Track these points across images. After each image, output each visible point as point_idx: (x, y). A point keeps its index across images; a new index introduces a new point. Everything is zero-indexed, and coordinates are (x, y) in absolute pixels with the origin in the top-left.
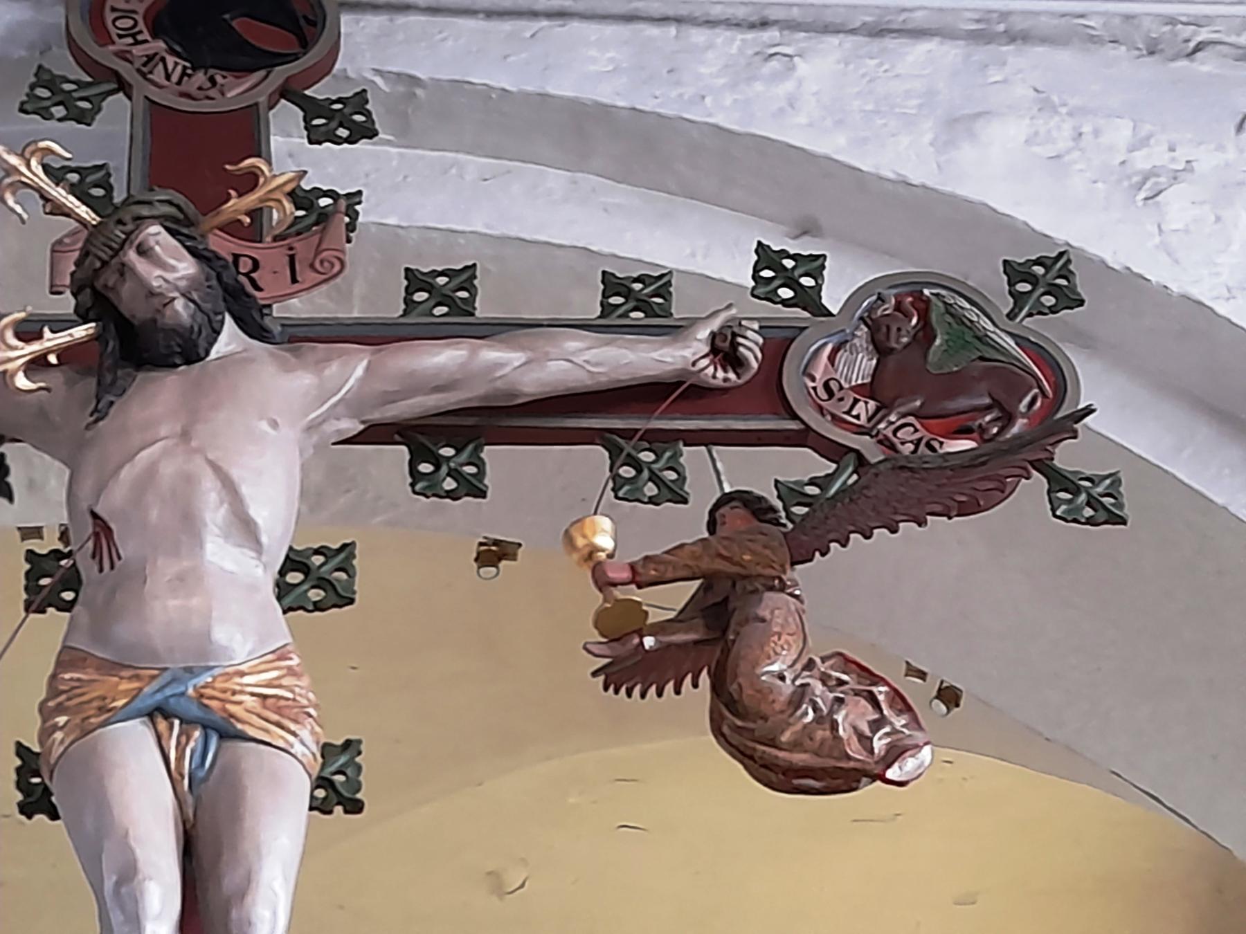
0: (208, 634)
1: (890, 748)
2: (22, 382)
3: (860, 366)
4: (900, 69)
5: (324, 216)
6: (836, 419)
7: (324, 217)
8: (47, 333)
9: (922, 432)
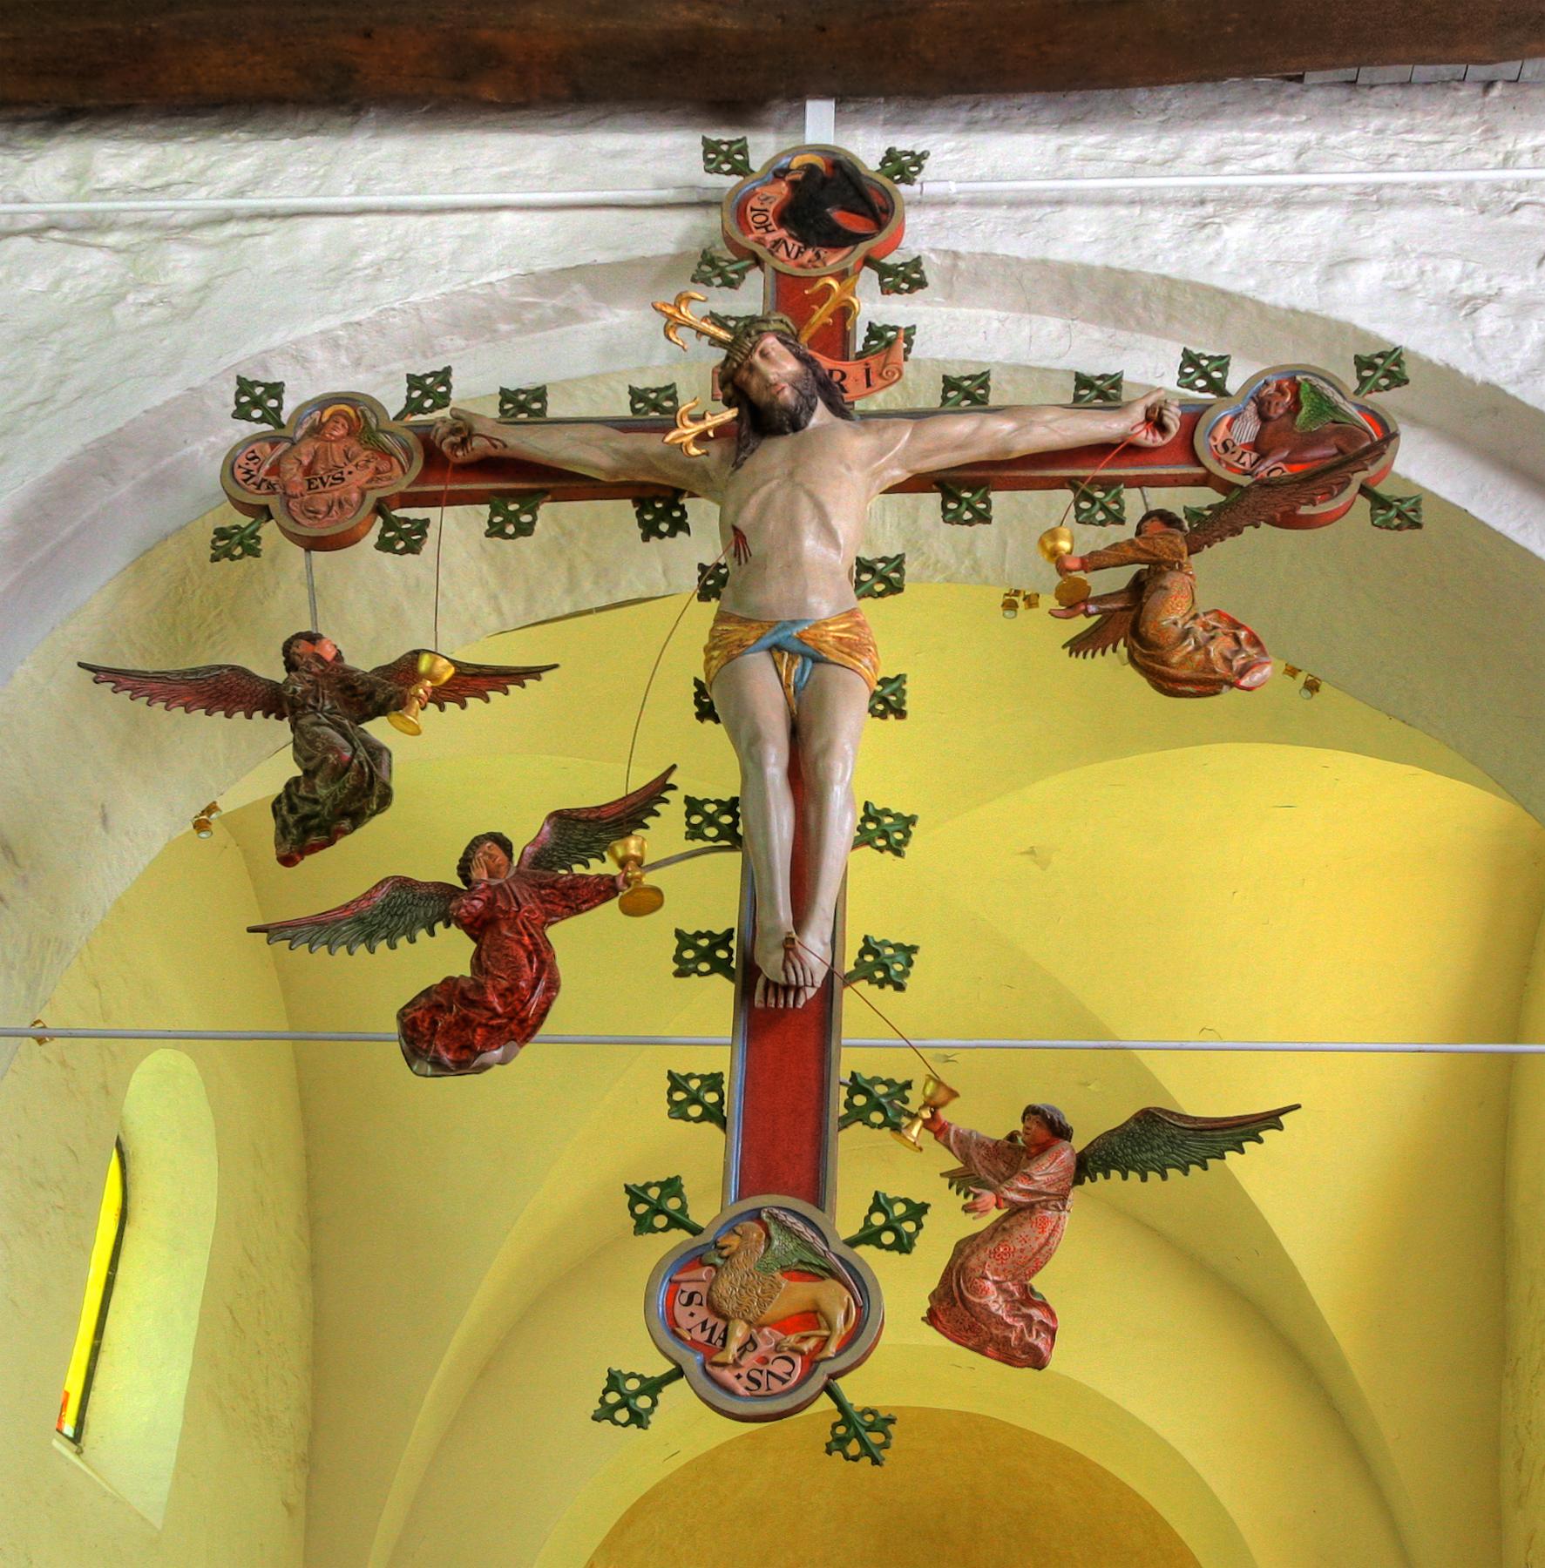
0: (805, 600)
2: (694, 451)
3: (1248, 429)
4: (1297, 231)
5: (887, 342)
6: (1229, 467)
7: (890, 343)
8: (708, 417)
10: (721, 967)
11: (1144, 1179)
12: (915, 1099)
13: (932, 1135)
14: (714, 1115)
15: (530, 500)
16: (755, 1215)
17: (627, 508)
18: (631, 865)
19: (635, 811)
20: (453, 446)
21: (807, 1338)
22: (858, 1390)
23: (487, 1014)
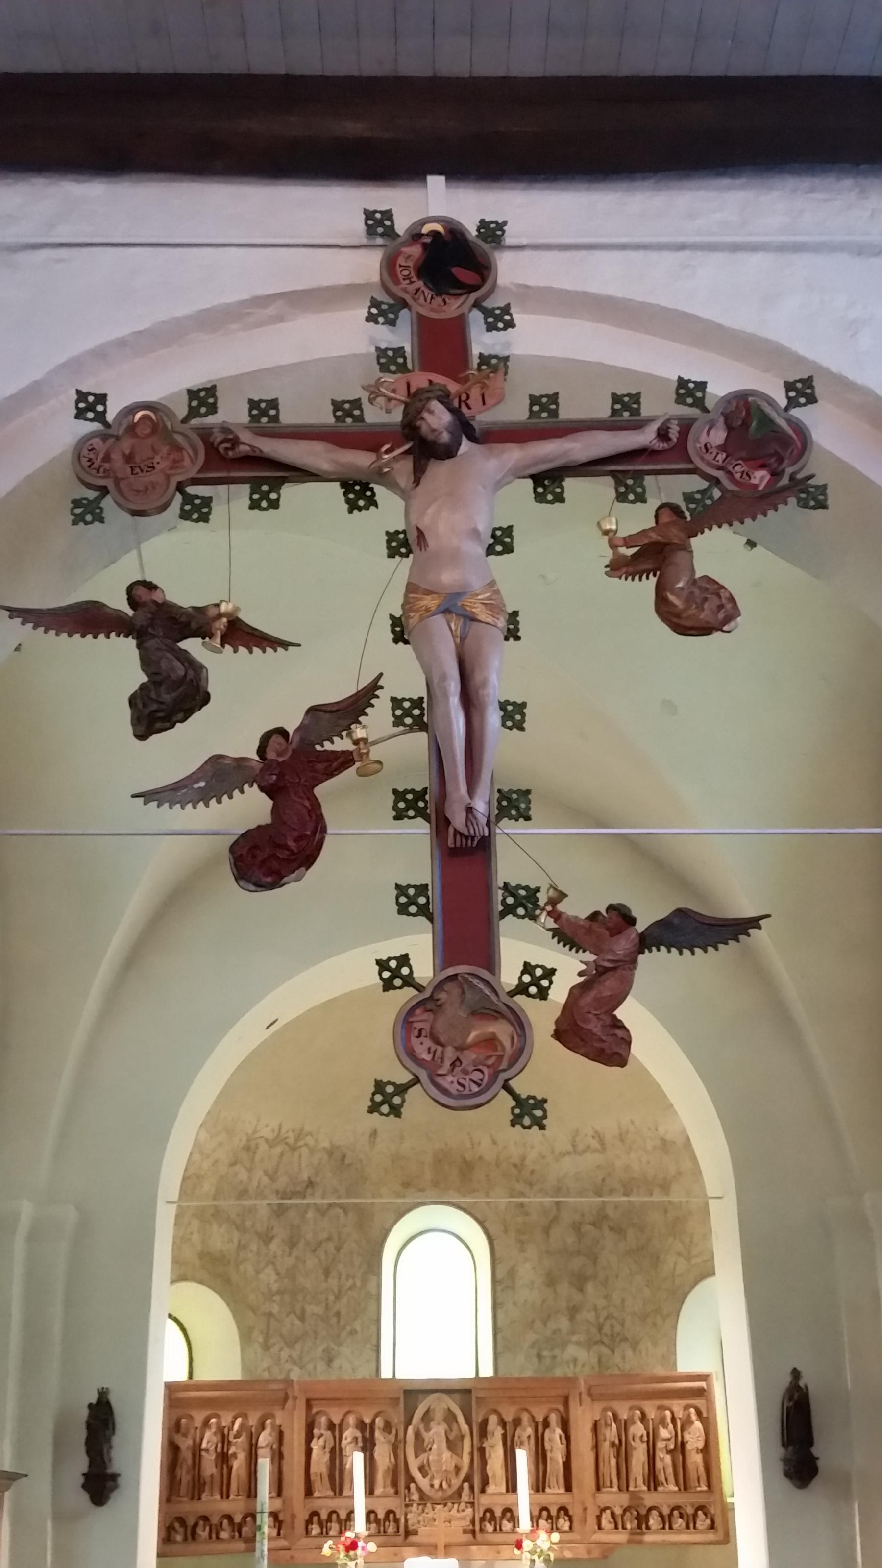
1: (726, 617)
3: (719, 436)
9: (745, 468)
10: (422, 813)
11: (681, 953)
12: (542, 898)
13: (552, 920)
14: (424, 911)
15: (276, 484)
16: (453, 978)
17: (337, 484)
18: (362, 745)
19: (356, 706)
20: (226, 449)
21: (491, 1056)
22: (523, 1085)
23: (287, 852)
